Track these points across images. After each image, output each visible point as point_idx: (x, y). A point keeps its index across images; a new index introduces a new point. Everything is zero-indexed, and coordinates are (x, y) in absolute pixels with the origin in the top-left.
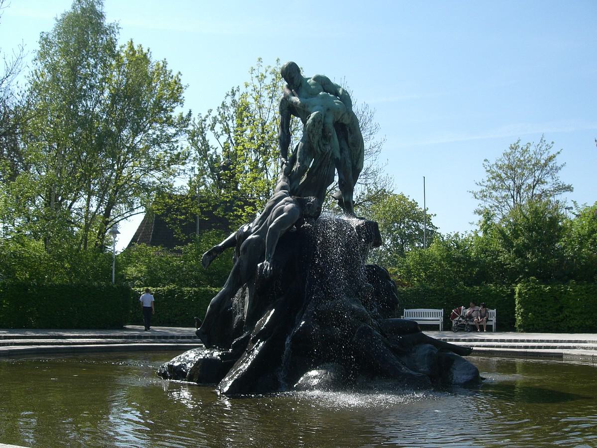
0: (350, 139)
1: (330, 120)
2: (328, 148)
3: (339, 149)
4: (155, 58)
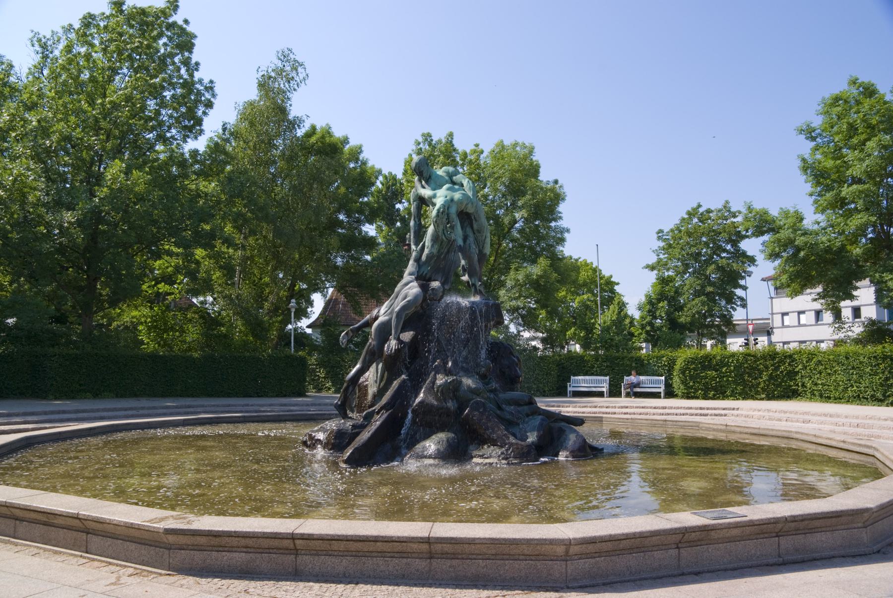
0: (475, 226)
1: (453, 210)
2: (453, 235)
3: (462, 237)
4: (690, 209)
